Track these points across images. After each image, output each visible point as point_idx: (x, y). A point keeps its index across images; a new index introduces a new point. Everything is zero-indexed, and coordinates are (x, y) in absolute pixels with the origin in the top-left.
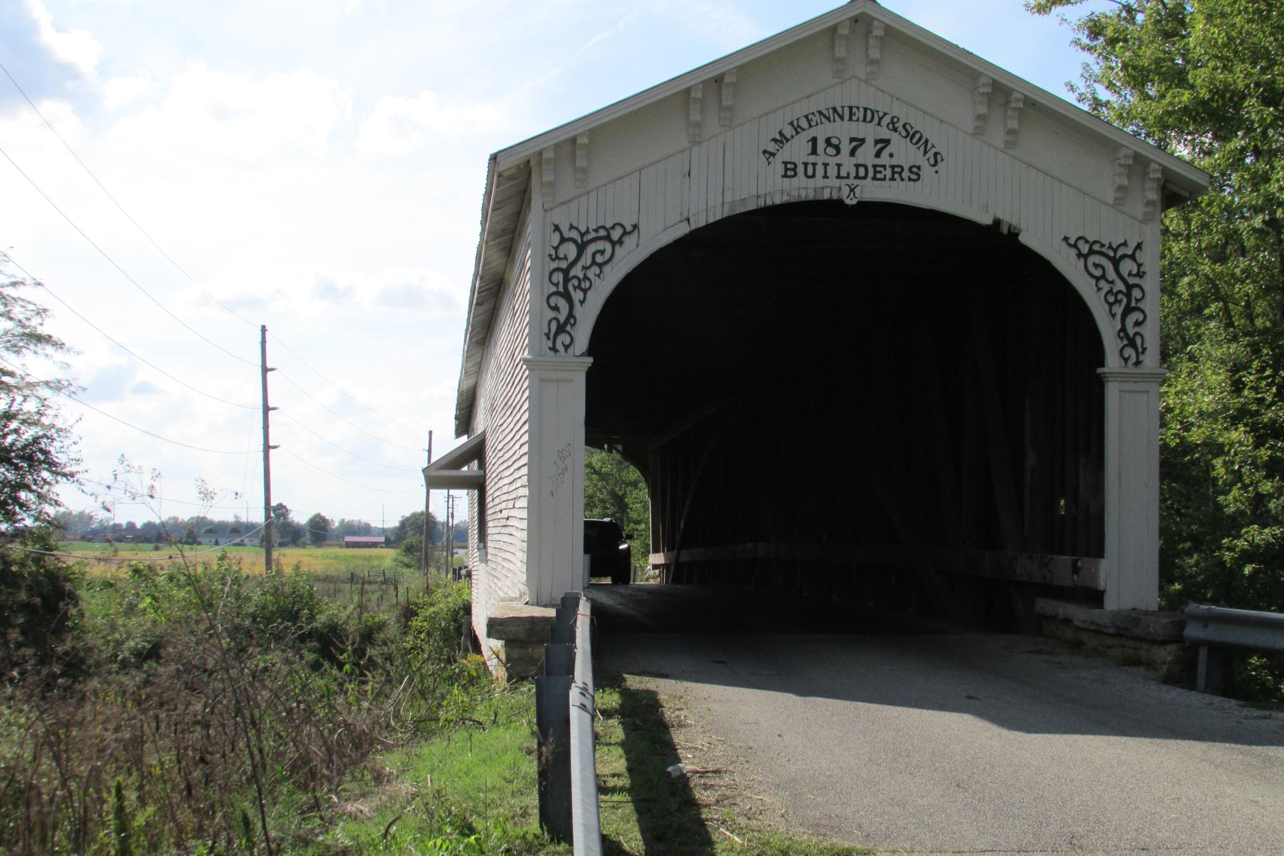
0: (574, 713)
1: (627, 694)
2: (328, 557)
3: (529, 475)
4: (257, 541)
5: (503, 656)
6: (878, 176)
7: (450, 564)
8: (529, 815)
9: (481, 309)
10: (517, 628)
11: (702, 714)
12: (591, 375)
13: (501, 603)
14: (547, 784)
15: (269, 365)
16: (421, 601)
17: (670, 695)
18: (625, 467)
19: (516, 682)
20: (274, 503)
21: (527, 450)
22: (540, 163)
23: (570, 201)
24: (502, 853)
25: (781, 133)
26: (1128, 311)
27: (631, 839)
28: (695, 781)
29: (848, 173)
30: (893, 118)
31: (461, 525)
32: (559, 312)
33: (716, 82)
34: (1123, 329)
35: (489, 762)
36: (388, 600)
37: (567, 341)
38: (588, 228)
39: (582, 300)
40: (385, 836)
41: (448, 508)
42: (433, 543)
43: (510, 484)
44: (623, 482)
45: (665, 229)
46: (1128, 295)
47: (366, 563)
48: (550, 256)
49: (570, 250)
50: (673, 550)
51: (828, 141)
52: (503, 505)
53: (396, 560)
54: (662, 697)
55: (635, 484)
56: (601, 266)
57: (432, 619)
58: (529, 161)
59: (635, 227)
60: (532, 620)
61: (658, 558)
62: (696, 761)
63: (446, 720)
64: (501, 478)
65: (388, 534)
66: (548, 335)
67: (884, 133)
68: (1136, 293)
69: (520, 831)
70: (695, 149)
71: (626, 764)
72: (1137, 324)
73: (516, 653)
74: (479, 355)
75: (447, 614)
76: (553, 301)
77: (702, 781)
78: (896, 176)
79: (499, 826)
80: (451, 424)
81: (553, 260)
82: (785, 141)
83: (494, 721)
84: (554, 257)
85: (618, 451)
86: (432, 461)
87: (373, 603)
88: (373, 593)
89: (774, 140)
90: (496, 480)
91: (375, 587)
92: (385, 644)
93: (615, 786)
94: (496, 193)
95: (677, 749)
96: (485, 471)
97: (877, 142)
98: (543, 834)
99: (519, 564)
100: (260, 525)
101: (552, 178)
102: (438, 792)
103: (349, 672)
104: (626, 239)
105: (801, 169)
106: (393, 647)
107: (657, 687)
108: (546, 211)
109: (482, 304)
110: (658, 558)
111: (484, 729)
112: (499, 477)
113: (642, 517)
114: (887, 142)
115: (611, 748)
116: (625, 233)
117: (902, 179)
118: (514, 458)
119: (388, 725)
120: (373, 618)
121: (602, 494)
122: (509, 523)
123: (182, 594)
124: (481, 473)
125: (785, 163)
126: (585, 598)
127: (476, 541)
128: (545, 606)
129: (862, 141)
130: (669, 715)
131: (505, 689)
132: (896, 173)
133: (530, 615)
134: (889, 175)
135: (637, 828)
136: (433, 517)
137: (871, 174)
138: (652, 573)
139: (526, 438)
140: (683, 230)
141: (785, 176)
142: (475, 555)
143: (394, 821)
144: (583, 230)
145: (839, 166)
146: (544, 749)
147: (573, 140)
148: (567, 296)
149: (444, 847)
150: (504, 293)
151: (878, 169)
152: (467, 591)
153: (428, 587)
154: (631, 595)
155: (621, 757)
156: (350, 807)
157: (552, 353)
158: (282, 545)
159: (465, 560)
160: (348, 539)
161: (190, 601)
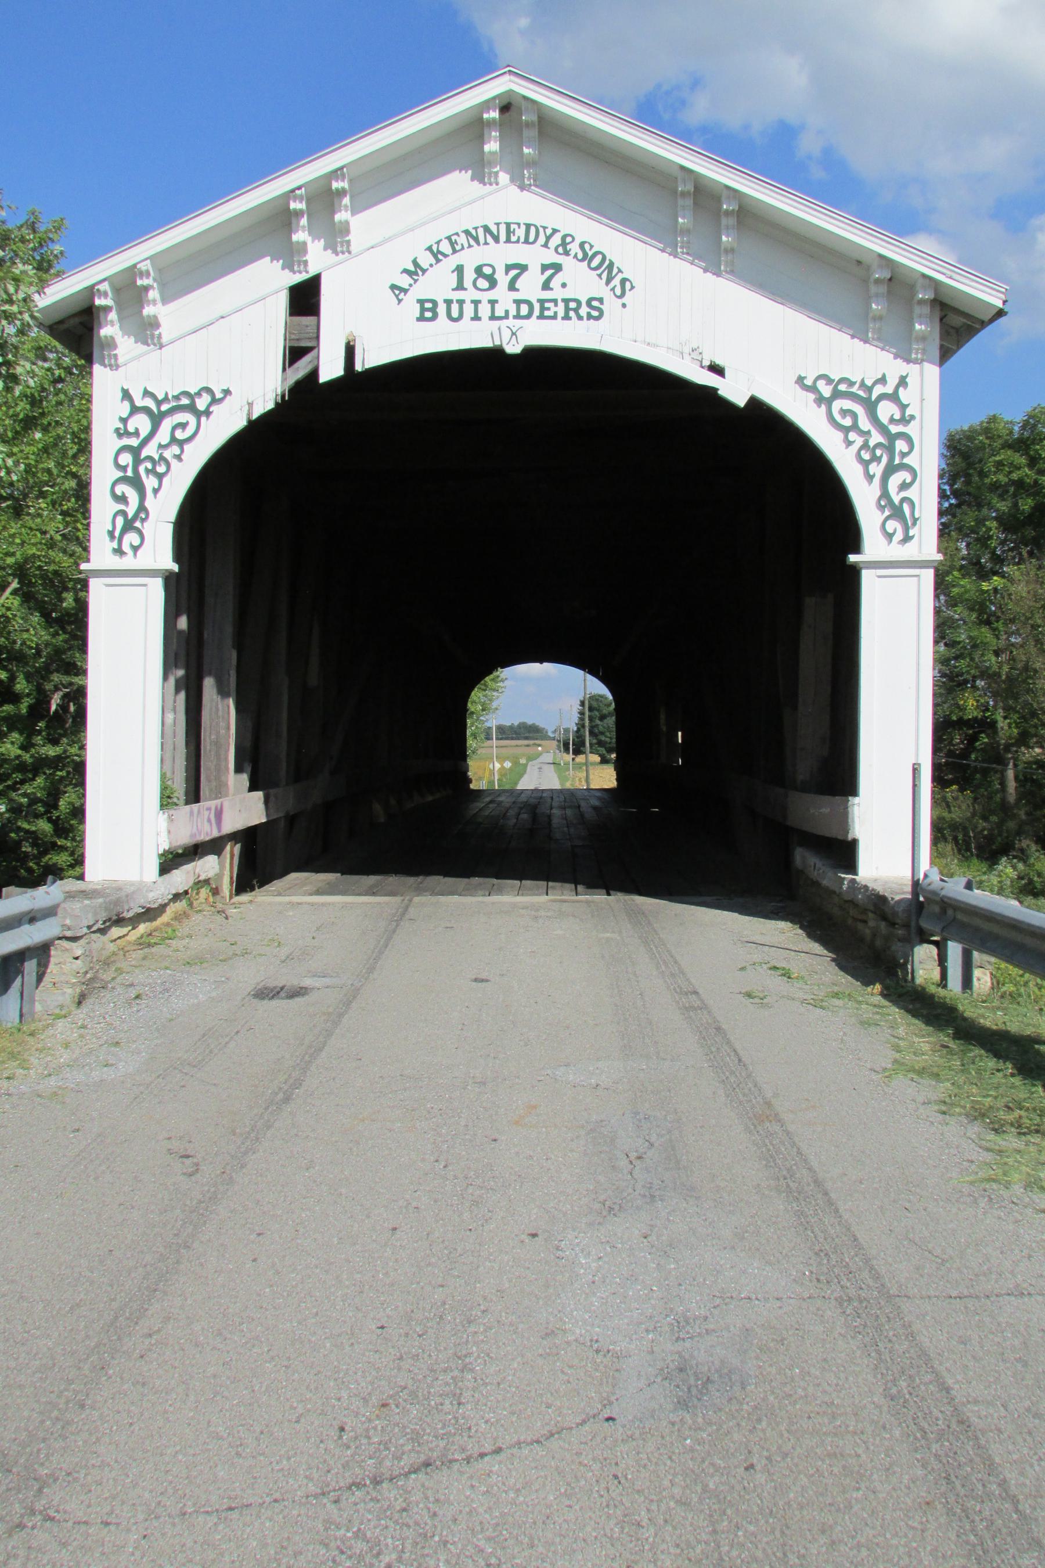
6: (547, 313)
25: (415, 263)
26: (890, 470)
29: (507, 312)
30: (564, 238)
34: (885, 494)
38: (167, 394)
46: (890, 449)
51: (479, 270)
56: (181, 443)
67: (550, 257)
68: (901, 445)
72: (904, 486)
76: (120, 489)
78: (572, 314)
82: (420, 273)
89: (406, 271)
97: (544, 268)
105: (442, 309)
114: (557, 268)
117: (580, 318)
125: (421, 302)
129: (523, 268)
132: (572, 309)
134: (561, 313)
137: (537, 312)
141: (421, 318)
145: (493, 303)
148: (136, 483)
151: (547, 305)
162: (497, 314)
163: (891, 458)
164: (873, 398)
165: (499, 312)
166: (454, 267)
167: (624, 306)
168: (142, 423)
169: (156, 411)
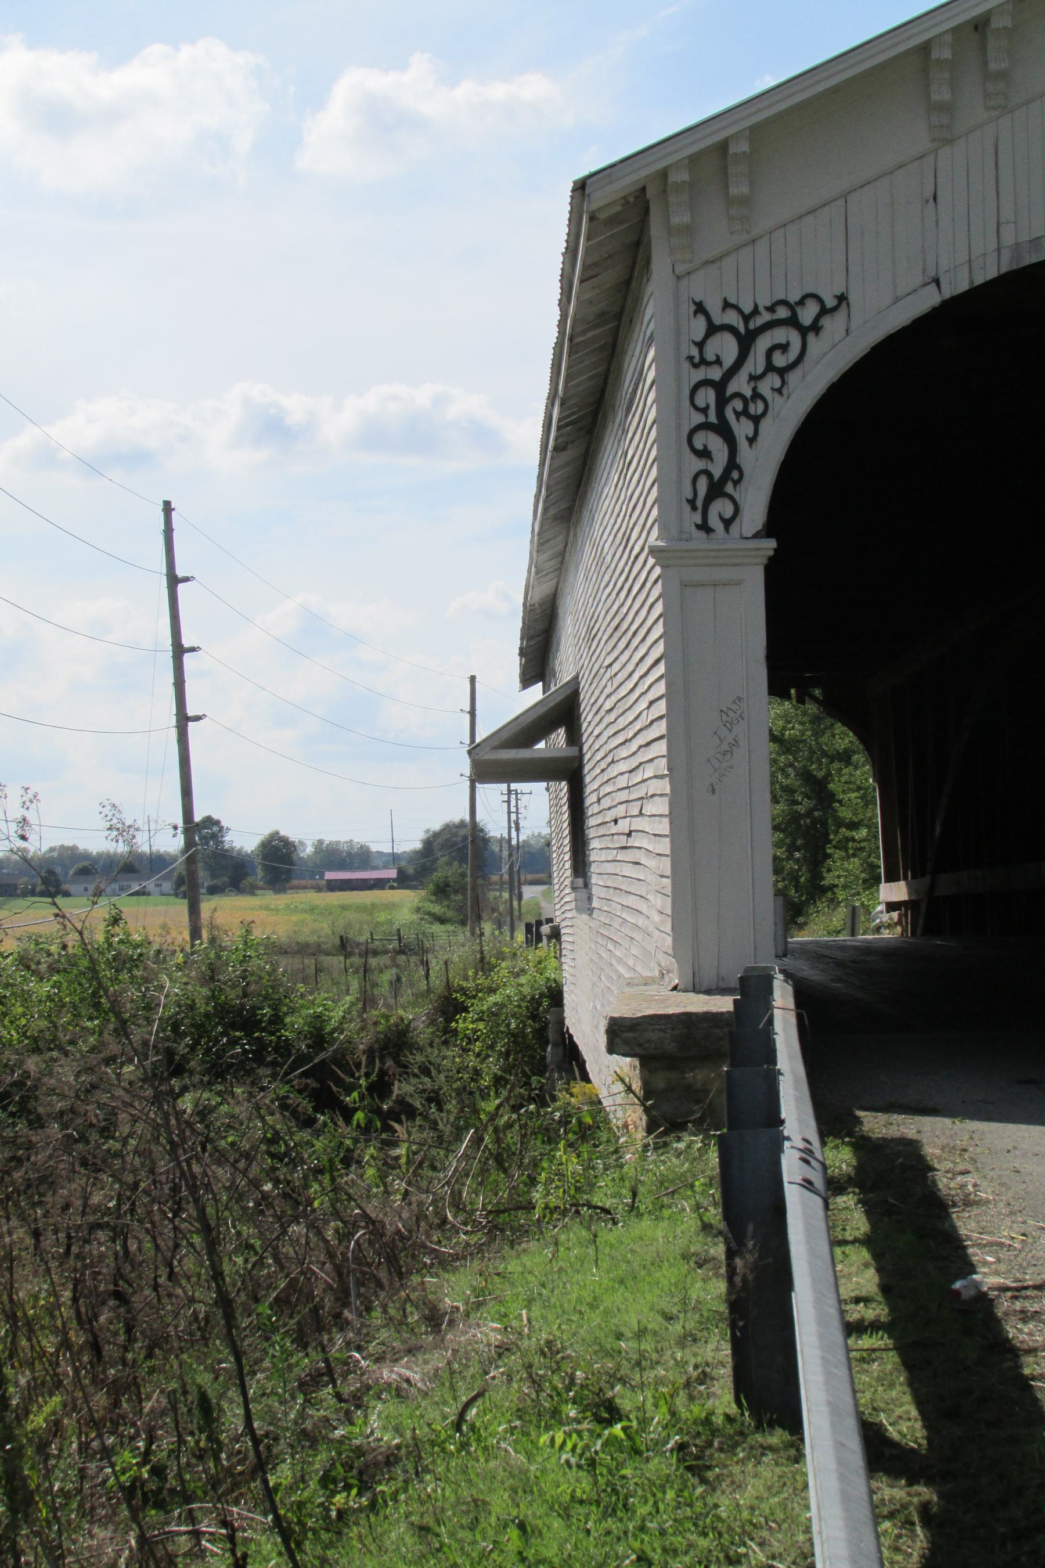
0: (794, 1197)
1: (865, 1146)
2: (296, 910)
3: (670, 756)
4: (167, 886)
5: (637, 1086)
7: (516, 913)
8: (712, 1379)
9: (565, 457)
10: (662, 1034)
11: (1005, 1180)
12: (774, 571)
13: (627, 990)
14: (745, 1325)
15: (180, 573)
16: (471, 984)
17: (943, 1148)
18: (826, 728)
19: (665, 1133)
20: (198, 818)
21: (664, 712)
22: (665, 191)
23: (721, 258)
24: (672, 1451)
27: (900, 1417)
28: (1004, 1305)
31: (532, 842)
32: (711, 459)
33: (976, 28)
35: (630, 1283)
36: (412, 985)
37: (728, 511)
38: (756, 306)
39: (751, 435)
40: (458, 1427)
41: (509, 813)
42: (485, 877)
43: (631, 772)
44: (824, 754)
45: (897, 300)
47: (366, 917)
48: (690, 358)
49: (727, 347)
50: (923, 875)
52: (620, 810)
53: (418, 910)
54: (930, 1151)
55: (845, 757)
56: (782, 372)
57: (493, 1015)
58: (643, 189)
59: (842, 298)
60: (688, 1020)
61: (896, 891)
62: (1002, 1267)
63: (547, 1207)
64: (613, 762)
65: (403, 864)
66: (692, 503)
69: (697, 1411)
70: (945, 152)
71: (876, 1279)
73: (660, 1081)
74: (561, 538)
75: (519, 1006)
76: (699, 442)
77: (1018, 1305)
79: (662, 1402)
80: (513, 664)
81: (696, 366)
83: (632, 1207)
84: (697, 360)
85: (814, 699)
86: (478, 740)
87: (385, 989)
88: (381, 971)
90: (603, 765)
91: (384, 960)
92: (426, 1071)
93: (862, 1320)
94: (587, 249)
95: (965, 1247)
96: (581, 749)
98: (743, 1414)
99: (657, 918)
100: (174, 859)
101: (686, 219)
102: (549, 1343)
103: (363, 1125)
104: (826, 322)
106: (442, 1077)
107: (919, 1132)
108: (679, 278)
109: (564, 449)
110: (896, 891)
111: (615, 1223)
112: (609, 759)
113: (861, 817)
115: (848, 1249)
116: (824, 311)
118: (638, 726)
119: (444, 1221)
120: (387, 1018)
121: (787, 776)
122: (632, 842)
123: (46, 988)
124: (573, 751)
126: (781, 977)
127: (569, 873)
128: (709, 992)
130: (945, 1184)
131: (646, 1147)
133: (682, 1010)
135: (908, 1398)
136: (482, 830)
138: (885, 918)
139: (661, 688)
140: (929, 300)
142: (567, 899)
143: (474, 1399)
144: (747, 309)
146: (738, 1262)
147: (723, 147)
149: (569, 1445)
150: (604, 427)
152: (554, 963)
153: (482, 959)
154: (853, 962)
155: (866, 1265)
156: (388, 1374)
157: (702, 535)
158: (213, 891)
159: (543, 904)
160: (329, 875)
161: (60, 1000)
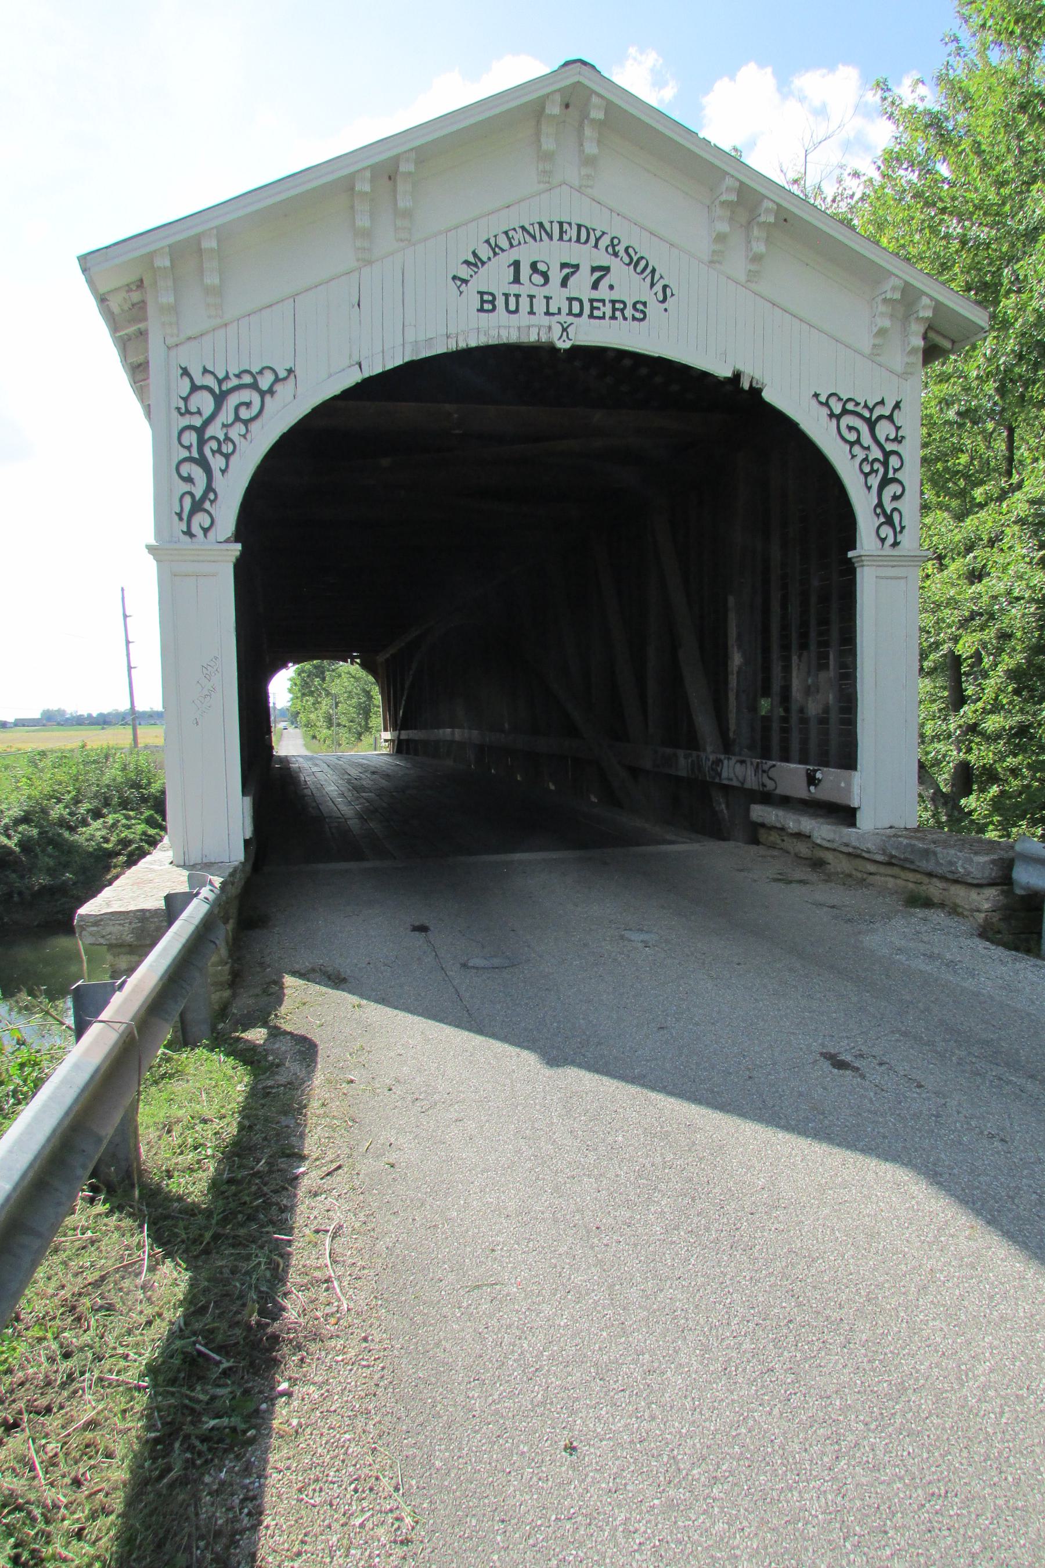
6: (596, 313)
26: (885, 482)
29: (559, 309)
30: (613, 239)
34: (880, 504)
46: (885, 464)
51: (534, 266)
56: (246, 422)
68: (894, 461)
72: (895, 498)
76: (185, 469)
78: (618, 314)
82: (479, 264)
89: (467, 263)
97: (594, 269)
117: (625, 319)
134: (609, 314)
141: (481, 310)
145: (548, 299)
148: (203, 463)
151: (595, 304)
162: (551, 311)
163: (886, 472)
164: (874, 418)
165: (553, 309)
166: (511, 262)
167: (666, 310)
168: (205, 402)
169: (217, 391)
